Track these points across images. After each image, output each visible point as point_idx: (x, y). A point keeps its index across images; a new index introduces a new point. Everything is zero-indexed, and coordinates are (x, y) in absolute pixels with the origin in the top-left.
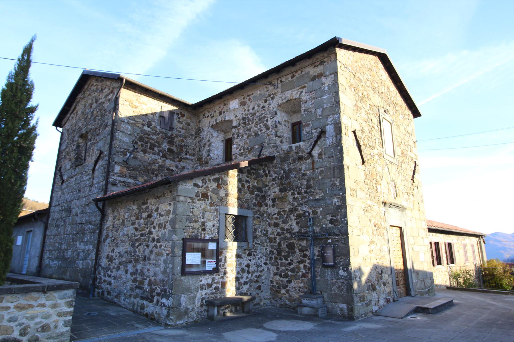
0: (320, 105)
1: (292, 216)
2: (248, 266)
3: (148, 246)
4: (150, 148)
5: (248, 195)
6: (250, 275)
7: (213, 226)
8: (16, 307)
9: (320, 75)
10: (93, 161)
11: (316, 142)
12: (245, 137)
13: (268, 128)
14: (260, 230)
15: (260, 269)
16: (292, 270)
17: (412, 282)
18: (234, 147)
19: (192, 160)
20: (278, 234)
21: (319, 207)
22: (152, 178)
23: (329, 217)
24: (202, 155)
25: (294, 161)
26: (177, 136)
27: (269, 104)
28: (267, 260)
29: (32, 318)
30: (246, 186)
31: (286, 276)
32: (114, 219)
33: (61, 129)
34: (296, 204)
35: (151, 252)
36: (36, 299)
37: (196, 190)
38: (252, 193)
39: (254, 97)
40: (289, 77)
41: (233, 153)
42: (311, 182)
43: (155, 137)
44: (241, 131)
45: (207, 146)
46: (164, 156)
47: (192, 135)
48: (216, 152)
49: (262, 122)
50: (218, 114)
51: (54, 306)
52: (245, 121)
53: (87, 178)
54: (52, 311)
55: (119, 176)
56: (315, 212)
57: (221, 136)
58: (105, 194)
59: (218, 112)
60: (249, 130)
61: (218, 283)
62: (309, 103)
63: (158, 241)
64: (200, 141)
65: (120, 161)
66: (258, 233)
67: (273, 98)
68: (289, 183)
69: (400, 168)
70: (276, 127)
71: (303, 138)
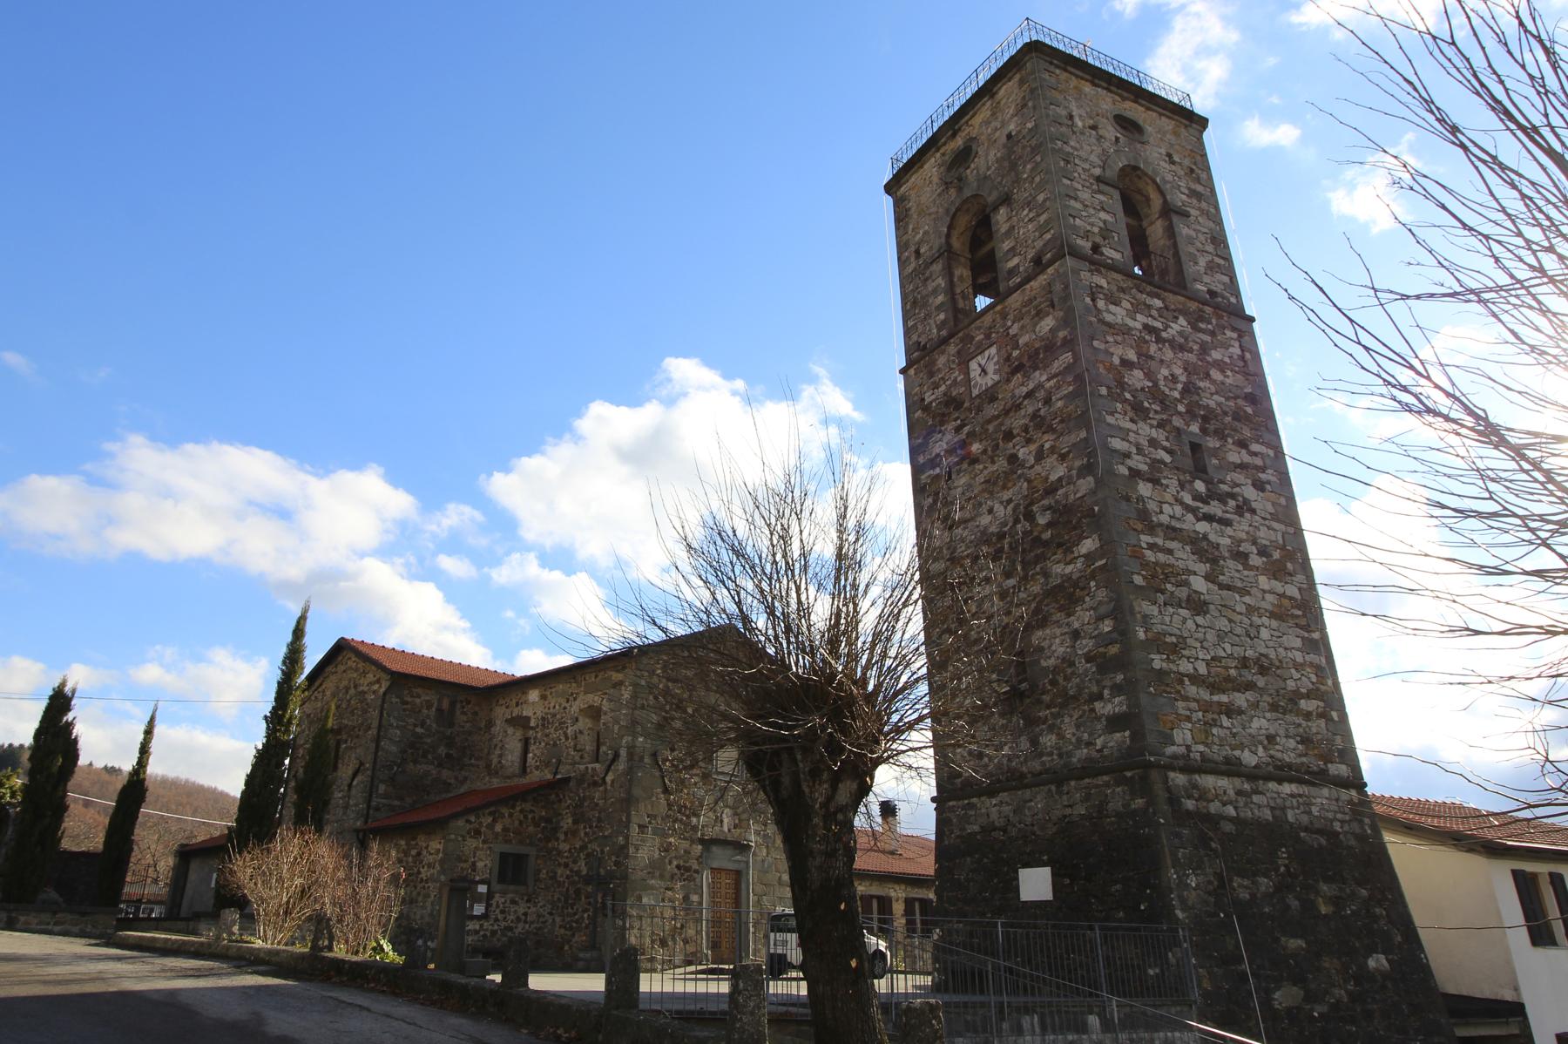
2: (525, 914)
3: (416, 887)
5: (531, 829)
6: (527, 926)
7: (486, 866)
10: (350, 772)
11: (610, 766)
12: (543, 744)
13: (567, 738)
14: (544, 871)
15: (541, 920)
16: (577, 922)
20: (568, 877)
23: (614, 858)
27: (571, 706)
28: (552, 909)
30: (530, 816)
31: (571, 928)
35: (419, 894)
37: (468, 826)
38: (537, 825)
40: (593, 675)
42: (603, 815)
43: (429, 741)
44: (539, 735)
45: (498, 748)
46: (440, 765)
53: (340, 795)
56: (602, 852)
57: (519, 734)
58: (366, 822)
59: (514, 701)
60: (547, 736)
61: (487, 930)
63: (427, 881)
64: (491, 739)
66: (543, 875)
67: (575, 699)
70: (576, 737)
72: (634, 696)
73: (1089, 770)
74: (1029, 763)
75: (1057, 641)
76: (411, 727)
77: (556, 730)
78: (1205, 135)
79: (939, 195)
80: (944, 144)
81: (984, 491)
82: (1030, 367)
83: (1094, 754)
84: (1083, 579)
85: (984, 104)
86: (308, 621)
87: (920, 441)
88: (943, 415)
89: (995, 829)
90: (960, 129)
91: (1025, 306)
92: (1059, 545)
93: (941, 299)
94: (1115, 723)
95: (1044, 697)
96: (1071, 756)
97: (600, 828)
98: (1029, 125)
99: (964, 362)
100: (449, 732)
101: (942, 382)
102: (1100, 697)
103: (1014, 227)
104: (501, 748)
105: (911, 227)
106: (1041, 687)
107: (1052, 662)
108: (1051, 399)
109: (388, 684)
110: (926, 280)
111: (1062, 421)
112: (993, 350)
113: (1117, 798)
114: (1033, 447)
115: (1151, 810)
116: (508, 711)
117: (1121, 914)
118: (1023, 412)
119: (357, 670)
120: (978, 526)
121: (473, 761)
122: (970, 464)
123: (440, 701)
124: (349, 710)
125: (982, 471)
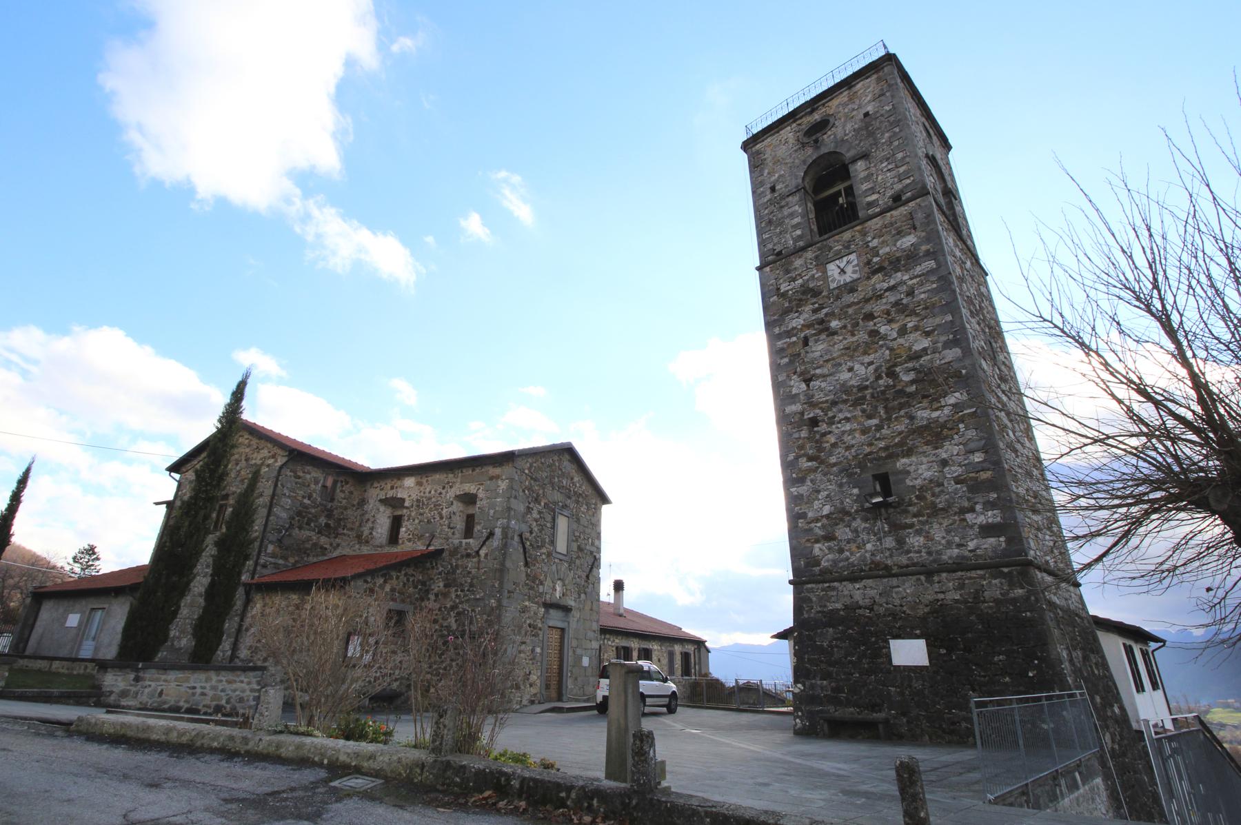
0: (492, 506)
1: (452, 613)
4: (307, 524)
5: (411, 590)
8: (226, 681)
9: (498, 477)
11: (484, 543)
12: (417, 521)
13: (441, 518)
17: (567, 687)
18: (403, 529)
19: (349, 536)
21: (478, 606)
22: (302, 558)
24: (362, 532)
25: (462, 557)
26: (336, 509)
27: (447, 492)
29: (235, 691)
32: (264, 606)
33: (177, 476)
34: (457, 601)
36: (238, 676)
37: (365, 586)
38: (415, 587)
39: (432, 480)
41: (400, 537)
42: (475, 581)
43: (313, 511)
44: (413, 514)
45: (370, 522)
46: (319, 532)
47: (354, 506)
48: (379, 530)
49: (437, 510)
50: (389, 488)
51: (249, 683)
52: (419, 503)
54: (247, 687)
55: (272, 557)
62: (484, 502)
64: (363, 515)
65: (274, 539)
67: (451, 487)
68: (455, 580)
69: (573, 565)
70: (450, 517)
71: (474, 535)
72: (511, 488)
73: (959, 566)
74: (895, 558)
75: (923, 466)
76: (300, 498)
77: (431, 510)
78: (950, 156)
79: (796, 151)
80: (801, 118)
81: (843, 355)
82: (891, 269)
83: (967, 553)
84: (951, 422)
85: (841, 93)
86: (248, 386)
87: (775, 317)
88: (800, 300)
89: (860, 608)
90: (817, 108)
91: (886, 227)
92: (924, 397)
93: (797, 220)
94: (988, 530)
95: (910, 508)
96: (941, 554)
97: (473, 592)
98: (887, 108)
99: (821, 263)
100: (329, 505)
101: (798, 277)
102: (972, 510)
103: (872, 174)
104: (373, 522)
105: (766, 171)
106: (907, 500)
107: (918, 482)
108: (914, 292)
109: (285, 459)
110: (782, 207)
111: (926, 308)
112: (853, 257)
113: (994, 588)
114: (896, 326)
115: (1033, 598)
116: (383, 493)
117: (1007, 679)
118: (884, 301)
119: (249, 446)
120: (837, 380)
121: (345, 531)
122: (828, 336)
123: (325, 479)
124: (239, 479)
125: (841, 341)
